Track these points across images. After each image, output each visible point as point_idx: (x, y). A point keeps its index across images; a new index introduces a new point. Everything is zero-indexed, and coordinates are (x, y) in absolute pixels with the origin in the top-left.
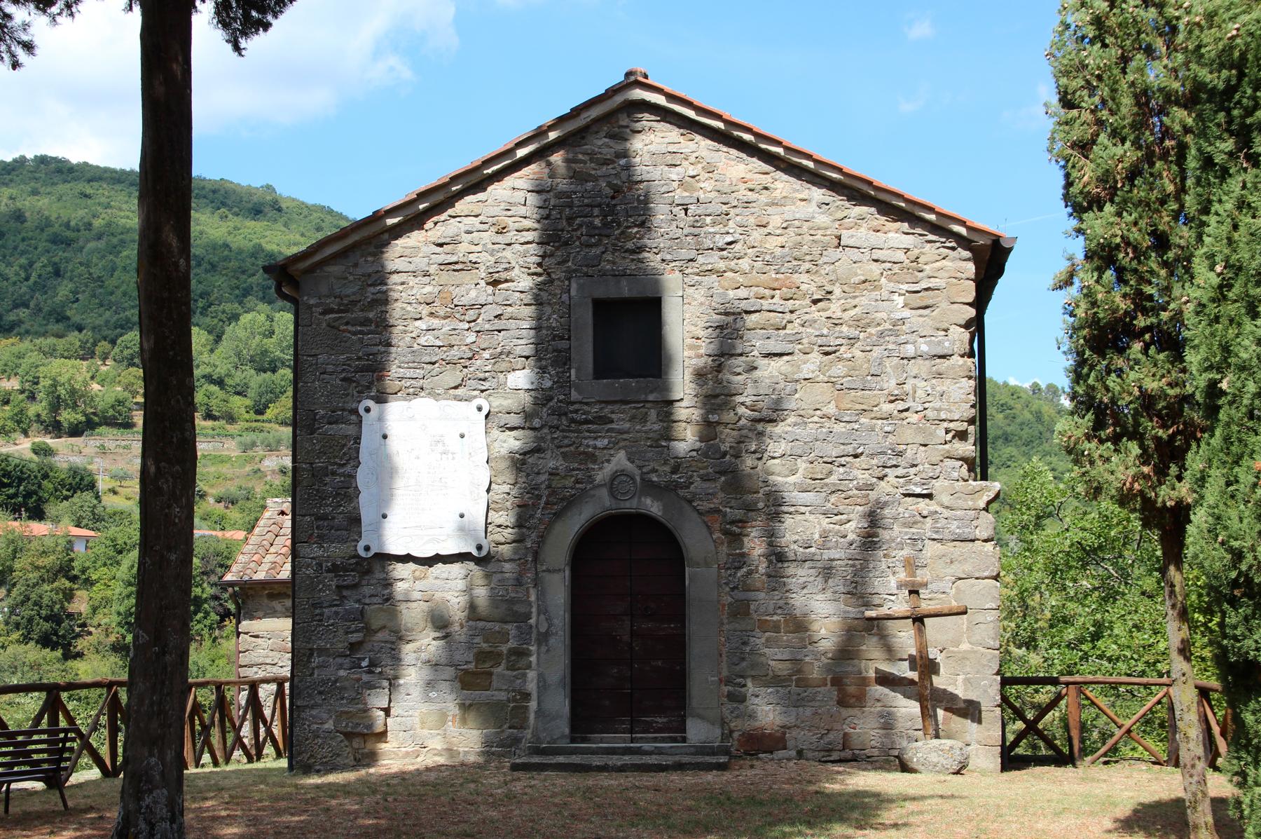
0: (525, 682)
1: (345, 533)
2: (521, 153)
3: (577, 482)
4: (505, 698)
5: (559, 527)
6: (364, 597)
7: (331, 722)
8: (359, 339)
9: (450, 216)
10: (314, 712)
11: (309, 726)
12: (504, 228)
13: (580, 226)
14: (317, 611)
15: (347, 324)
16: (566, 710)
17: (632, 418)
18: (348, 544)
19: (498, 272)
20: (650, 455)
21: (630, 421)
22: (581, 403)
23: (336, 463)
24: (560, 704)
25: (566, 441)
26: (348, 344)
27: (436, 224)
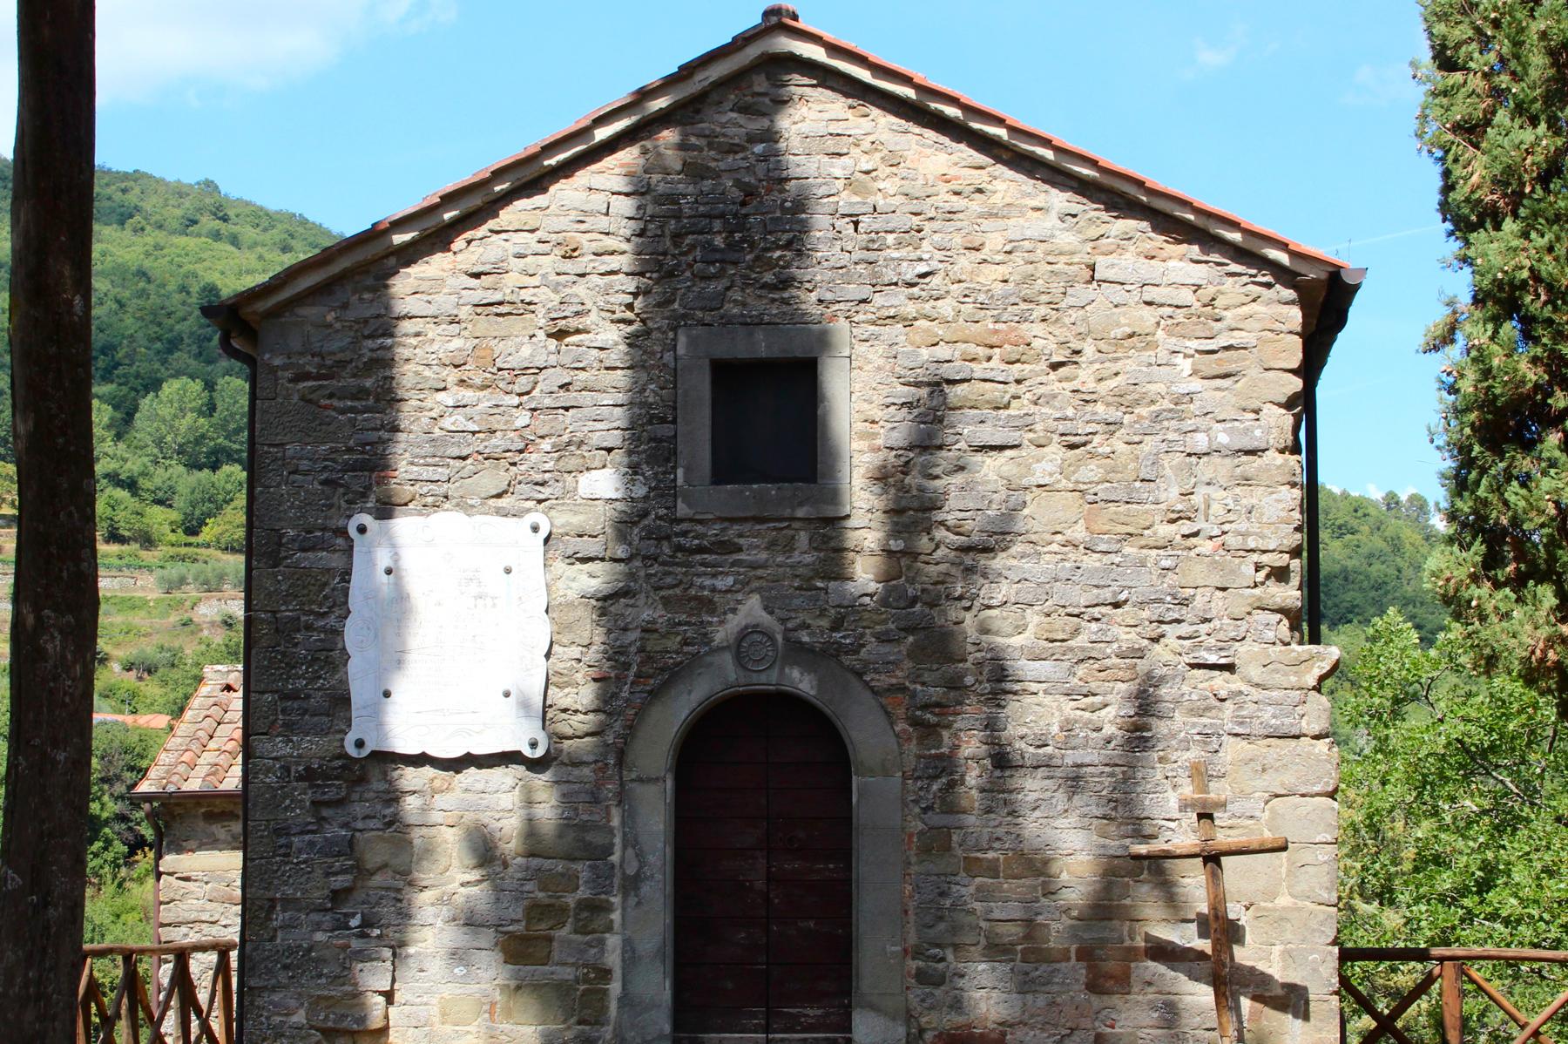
0: (602, 951)
1: (325, 719)
2: (602, 134)
3: (685, 643)
4: (571, 977)
5: (656, 713)
6: (355, 819)
7: (302, 1012)
8: (350, 420)
9: (491, 231)
10: (276, 997)
11: (268, 1018)
12: (574, 250)
13: (692, 247)
14: (282, 841)
15: (331, 396)
16: (666, 995)
17: (771, 545)
18: (331, 737)
19: (565, 318)
20: (797, 602)
21: (767, 548)
22: (691, 520)
23: (312, 612)
24: (657, 986)
25: (669, 580)
26: (331, 428)
27: (469, 242)
